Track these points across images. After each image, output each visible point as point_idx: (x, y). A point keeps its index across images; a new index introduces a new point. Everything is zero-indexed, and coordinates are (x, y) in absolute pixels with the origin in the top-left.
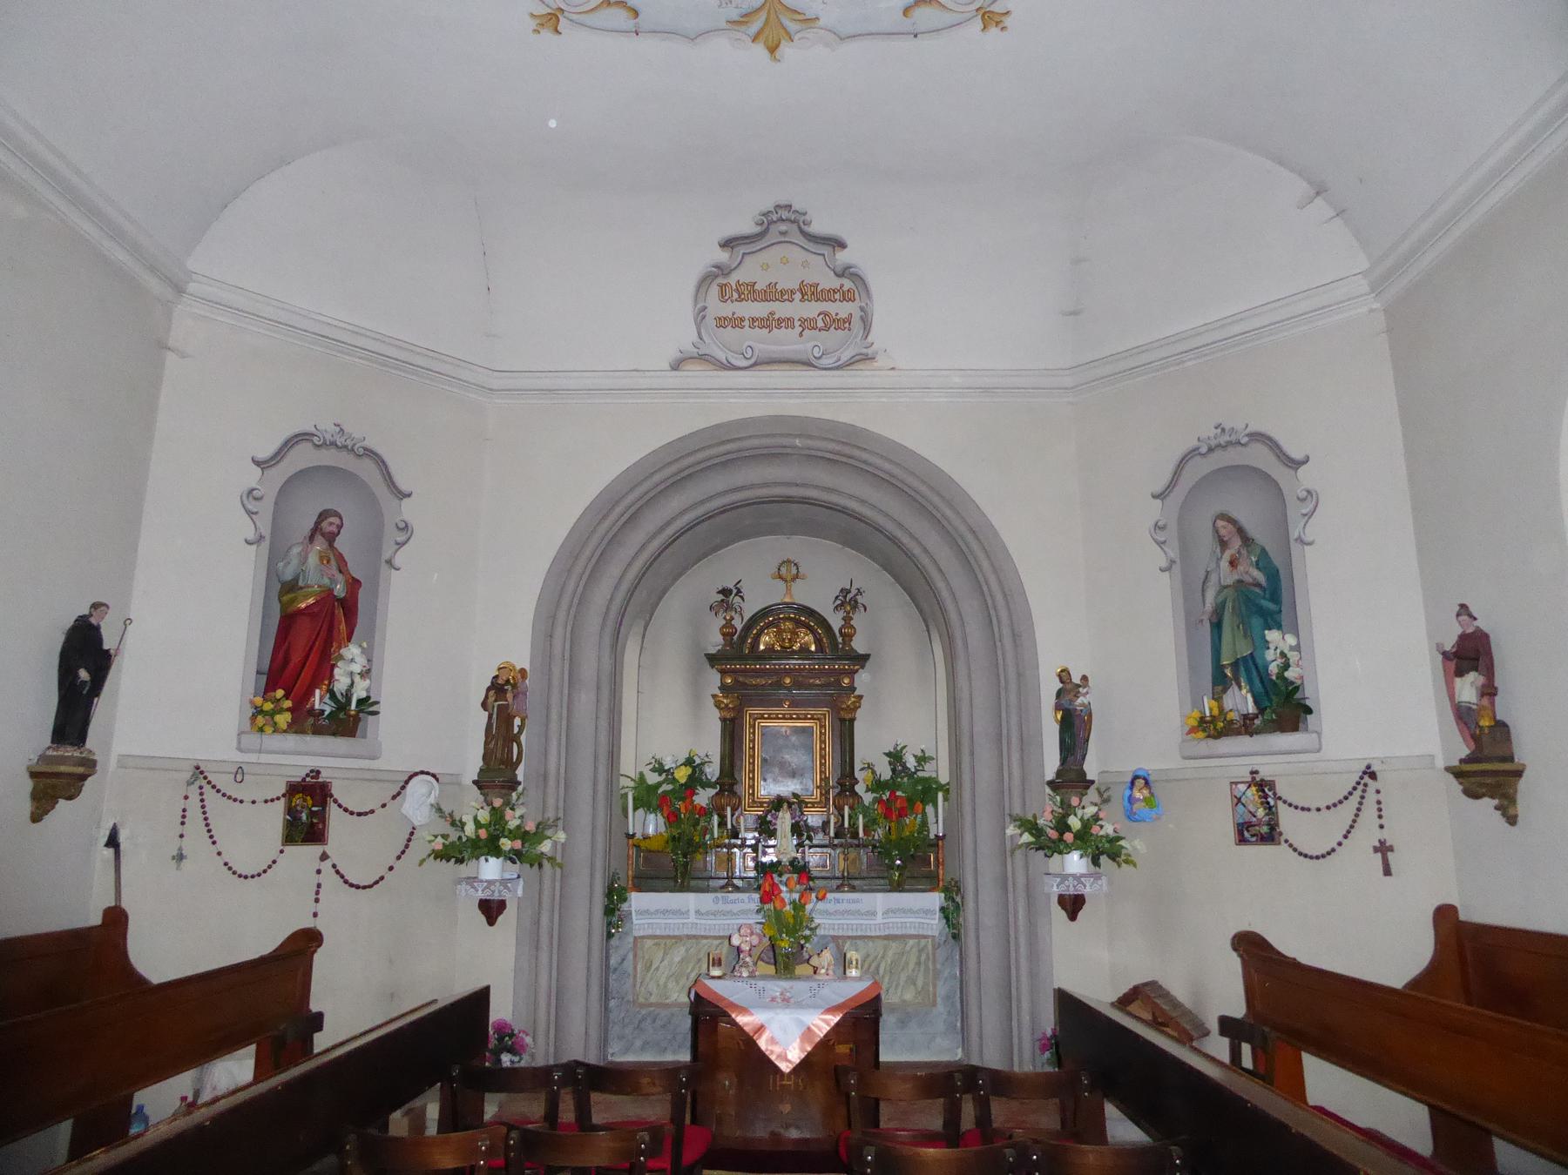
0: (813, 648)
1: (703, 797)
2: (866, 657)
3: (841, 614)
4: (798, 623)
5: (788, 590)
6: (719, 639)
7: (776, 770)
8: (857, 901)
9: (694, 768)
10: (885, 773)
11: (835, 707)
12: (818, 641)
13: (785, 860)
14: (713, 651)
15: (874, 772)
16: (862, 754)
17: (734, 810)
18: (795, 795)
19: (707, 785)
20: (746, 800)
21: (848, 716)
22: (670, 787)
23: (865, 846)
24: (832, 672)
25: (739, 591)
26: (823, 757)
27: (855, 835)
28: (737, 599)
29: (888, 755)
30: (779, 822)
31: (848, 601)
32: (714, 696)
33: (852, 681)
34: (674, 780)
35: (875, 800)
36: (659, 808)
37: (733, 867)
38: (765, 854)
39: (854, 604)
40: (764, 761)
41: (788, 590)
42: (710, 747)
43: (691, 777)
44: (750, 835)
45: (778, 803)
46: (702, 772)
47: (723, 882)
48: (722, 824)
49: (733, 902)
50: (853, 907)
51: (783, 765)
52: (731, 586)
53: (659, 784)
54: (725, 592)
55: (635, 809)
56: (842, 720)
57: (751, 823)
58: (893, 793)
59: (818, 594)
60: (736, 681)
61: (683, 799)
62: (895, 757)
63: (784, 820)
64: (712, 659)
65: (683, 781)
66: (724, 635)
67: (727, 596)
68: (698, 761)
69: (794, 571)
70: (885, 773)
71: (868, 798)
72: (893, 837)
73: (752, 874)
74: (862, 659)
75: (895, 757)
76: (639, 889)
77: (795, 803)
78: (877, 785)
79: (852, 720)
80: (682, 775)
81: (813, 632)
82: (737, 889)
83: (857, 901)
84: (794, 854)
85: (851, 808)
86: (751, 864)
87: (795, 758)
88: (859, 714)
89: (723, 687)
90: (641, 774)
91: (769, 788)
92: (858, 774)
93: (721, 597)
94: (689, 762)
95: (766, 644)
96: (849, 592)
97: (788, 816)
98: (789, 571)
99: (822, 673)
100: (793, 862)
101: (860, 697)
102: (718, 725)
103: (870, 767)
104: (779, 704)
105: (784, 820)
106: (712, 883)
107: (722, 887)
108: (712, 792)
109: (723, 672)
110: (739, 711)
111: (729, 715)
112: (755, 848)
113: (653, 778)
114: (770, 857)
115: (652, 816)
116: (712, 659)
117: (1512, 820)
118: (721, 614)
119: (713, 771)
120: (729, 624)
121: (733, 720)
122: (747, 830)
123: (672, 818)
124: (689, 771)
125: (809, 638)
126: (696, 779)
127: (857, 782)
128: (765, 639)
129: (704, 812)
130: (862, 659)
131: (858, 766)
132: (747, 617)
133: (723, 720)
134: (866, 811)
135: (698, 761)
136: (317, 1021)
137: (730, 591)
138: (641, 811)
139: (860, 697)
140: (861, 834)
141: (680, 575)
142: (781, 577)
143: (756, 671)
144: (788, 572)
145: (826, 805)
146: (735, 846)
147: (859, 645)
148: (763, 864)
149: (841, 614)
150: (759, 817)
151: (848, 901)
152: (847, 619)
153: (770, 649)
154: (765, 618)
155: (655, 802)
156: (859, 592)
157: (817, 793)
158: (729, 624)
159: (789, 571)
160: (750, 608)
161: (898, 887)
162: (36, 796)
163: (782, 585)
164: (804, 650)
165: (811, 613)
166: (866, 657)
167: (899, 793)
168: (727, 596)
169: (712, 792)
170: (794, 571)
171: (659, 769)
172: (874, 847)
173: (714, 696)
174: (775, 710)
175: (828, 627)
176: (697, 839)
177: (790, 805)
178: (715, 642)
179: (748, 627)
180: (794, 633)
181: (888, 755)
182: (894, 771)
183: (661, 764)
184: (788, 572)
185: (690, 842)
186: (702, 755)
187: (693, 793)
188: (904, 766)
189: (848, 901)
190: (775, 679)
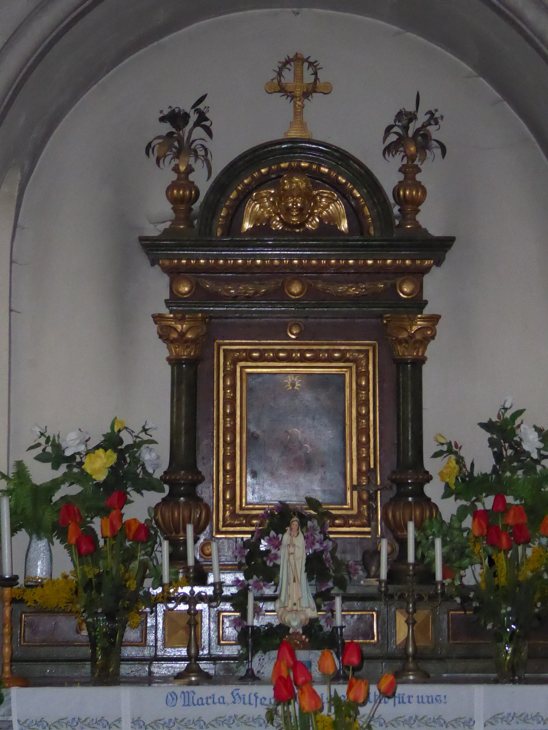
0: (344, 225)
1: (140, 507)
2: (445, 244)
3: (397, 161)
4: (316, 179)
5: (298, 113)
6: (165, 209)
7: (275, 456)
8: (437, 699)
9: (121, 454)
10: (483, 461)
11: (385, 339)
12: (354, 214)
13: (295, 623)
14: (153, 231)
15: (460, 461)
16: (435, 426)
17: (198, 532)
18: (312, 503)
19: (146, 484)
20: (220, 513)
21: (409, 354)
22: (75, 490)
23: (447, 598)
24: (378, 272)
25: (202, 117)
26: (363, 431)
27: (428, 576)
28: (199, 132)
29: (488, 426)
30: (283, 552)
31: (412, 137)
32: (158, 318)
33: (420, 288)
34: (84, 477)
35: (462, 513)
36: (59, 531)
37: (198, 638)
38: (257, 612)
39: (423, 140)
40: (252, 438)
41: (298, 113)
42: (151, 412)
43: (113, 470)
44: (228, 578)
45: (280, 518)
46: (137, 461)
47: (182, 666)
48: (178, 556)
49: (201, 702)
50: (427, 710)
51: (288, 447)
52: (186, 105)
53: (55, 485)
54: (176, 118)
55: (14, 530)
56: (400, 363)
57: (228, 555)
58: (500, 500)
59: (352, 120)
60: (196, 287)
61: (103, 512)
62: (501, 431)
63: (293, 551)
64: (152, 247)
65: (101, 477)
66: (175, 201)
67: (181, 129)
68: (127, 439)
69: (309, 78)
70: (483, 461)
71: (448, 508)
72: (502, 580)
73: (233, 650)
74: (438, 248)
75: (501, 431)
76: (26, 682)
77: (311, 516)
78: (467, 485)
79: (422, 360)
80: (99, 466)
81: (344, 195)
82: (206, 679)
83: (437, 699)
84: (312, 613)
85: (419, 527)
86: (230, 632)
87: (316, 435)
88: (432, 350)
89: (174, 300)
90: (20, 464)
91: (260, 492)
92: (431, 465)
93: (167, 128)
94: (111, 442)
95: (256, 219)
96: (412, 117)
97: (300, 541)
98: (299, 77)
99: (361, 274)
100: (311, 627)
101: (435, 319)
102: (165, 372)
103: (451, 449)
104: (278, 331)
105: (293, 551)
106: (161, 669)
107: (179, 676)
108: (154, 498)
109: (175, 274)
110: (205, 344)
111: (185, 353)
112: (239, 602)
113: (42, 474)
114: (265, 618)
115: (42, 544)
116: (152, 247)
117: (212, 139)
118: (169, 163)
119: (156, 458)
120: (183, 180)
121: (193, 362)
122: (224, 568)
123: (85, 548)
124: (111, 458)
125: (338, 207)
126: (125, 476)
127: (429, 478)
128: (254, 208)
129: (144, 534)
130: (438, 248)
131: (429, 447)
132: (219, 165)
133: (175, 362)
134: (447, 531)
135: (127, 439)
136: (139, 491)
137: (186, 116)
138: (23, 535)
139: (435, 319)
140: (439, 576)
141: (85, 86)
142: (282, 90)
143: (235, 269)
144: (298, 79)
145: (370, 521)
146: (201, 598)
147: (431, 219)
148: (256, 630)
149: (397, 161)
150: (246, 544)
151: (420, 700)
152: (409, 171)
153: (262, 229)
154: (260, 164)
155: (49, 517)
156: (433, 118)
157: (352, 497)
158: (183, 180)
159: (299, 77)
160: (225, 148)
161: (512, 674)
162: (450, 246)
163: (282, 103)
164: (328, 228)
165: (341, 158)
166: (445, 244)
167: (510, 499)
168: (181, 129)
169: (154, 498)
170: (309, 78)
171: (55, 455)
172: (465, 599)
173: (158, 318)
174: (273, 344)
175: (366, 179)
176: (132, 585)
177: (303, 519)
178: (157, 213)
179: (220, 187)
180: (309, 198)
181: (488, 426)
182: (498, 456)
183: (57, 447)
184: (298, 79)
185: (120, 589)
186: (137, 429)
187: (123, 500)
188: (517, 447)
189: (420, 700)
190: (272, 284)
